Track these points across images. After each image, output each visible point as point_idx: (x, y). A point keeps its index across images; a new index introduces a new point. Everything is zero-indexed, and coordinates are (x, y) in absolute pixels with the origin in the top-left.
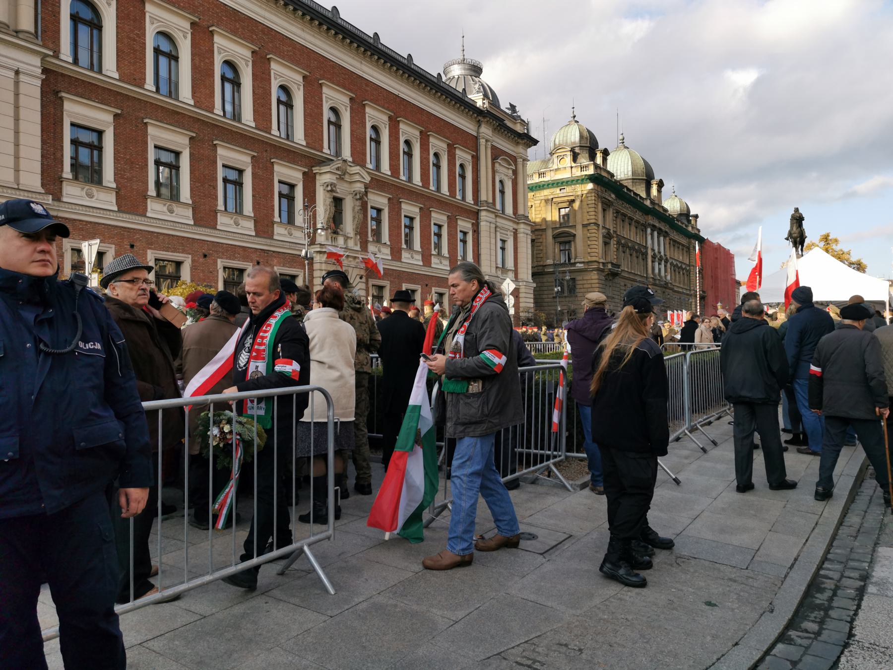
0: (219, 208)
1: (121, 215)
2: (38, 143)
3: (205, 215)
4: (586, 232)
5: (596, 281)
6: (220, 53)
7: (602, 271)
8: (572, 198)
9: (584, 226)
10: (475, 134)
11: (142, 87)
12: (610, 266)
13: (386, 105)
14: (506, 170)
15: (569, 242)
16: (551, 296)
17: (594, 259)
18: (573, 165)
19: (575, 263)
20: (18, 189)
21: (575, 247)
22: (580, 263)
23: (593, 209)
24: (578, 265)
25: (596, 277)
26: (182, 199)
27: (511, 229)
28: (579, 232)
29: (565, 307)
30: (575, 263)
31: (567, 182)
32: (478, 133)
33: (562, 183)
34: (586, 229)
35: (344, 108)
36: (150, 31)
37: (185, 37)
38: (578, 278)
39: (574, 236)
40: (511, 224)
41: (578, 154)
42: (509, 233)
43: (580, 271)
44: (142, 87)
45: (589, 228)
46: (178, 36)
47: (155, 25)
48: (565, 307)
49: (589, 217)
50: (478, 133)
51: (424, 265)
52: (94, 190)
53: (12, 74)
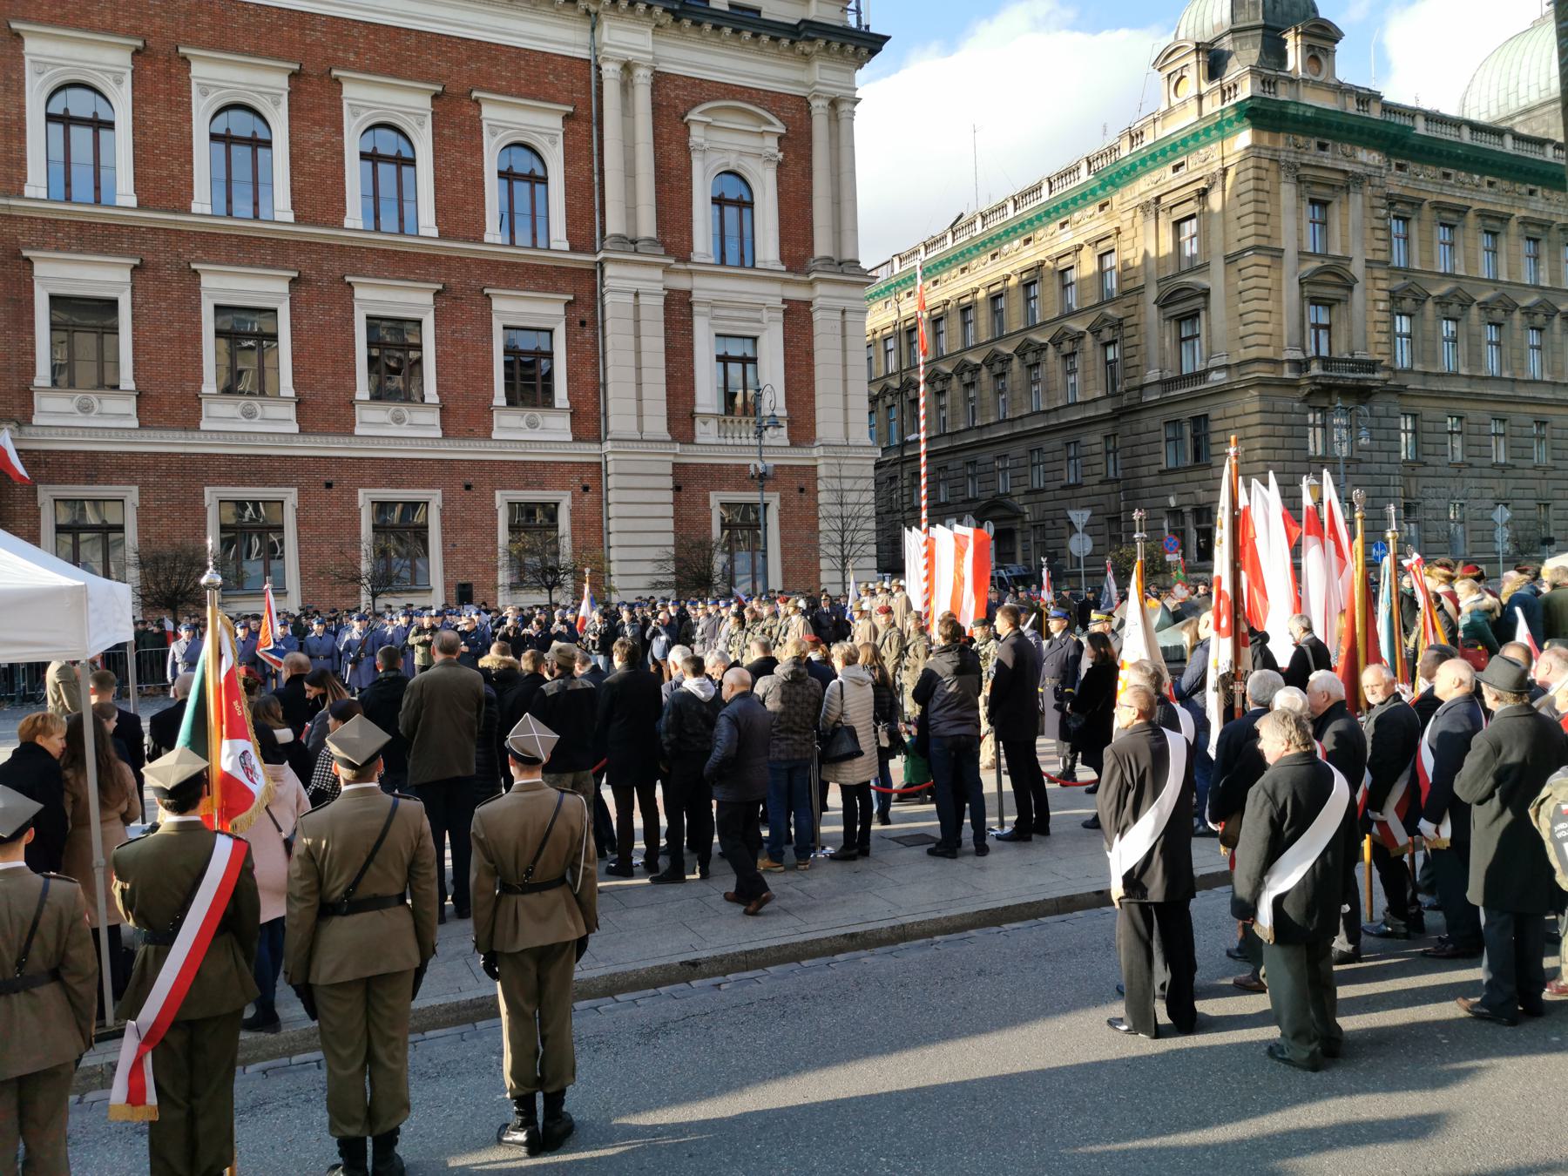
0: (495, 403)
1: (145, 433)
2: (819, 387)
3: (167, 402)
4: (1234, 278)
5: (1256, 419)
6: (494, 134)
7: (1291, 385)
8: (1202, 184)
9: (1230, 260)
10: (583, 54)
11: (480, 240)
12: (1315, 369)
13: (124, 24)
14: (754, 142)
15: (1193, 316)
16: (1155, 469)
17: (1253, 353)
18: (1205, 87)
19: (1207, 372)
20: (642, 440)
21: (1209, 325)
22: (1218, 369)
23: (1250, 208)
24: (1214, 376)
25: (1255, 406)
26: (557, 405)
27: (777, 302)
28: (1216, 280)
29: (1185, 499)
30: (1207, 372)
31: (1184, 142)
32: (594, 48)
33: (1174, 147)
34: (1233, 269)
35: (413, 121)
36: (201, 111)
37: (554, 143)
38: (1214, 415)
39: (1206, 293)
40: (776, 289)
41: (1230, 54)
42: (765, 315)
43: (1220, 392)
44: (480, 240)
45: (1241, 263)
46: (541, 144)
47: (210, 98)
48: (1185, 499)
49: (1240, 233)
50: (594, 48)
51: (675, 440)
52: (538, 414)
53: (630, 299)
